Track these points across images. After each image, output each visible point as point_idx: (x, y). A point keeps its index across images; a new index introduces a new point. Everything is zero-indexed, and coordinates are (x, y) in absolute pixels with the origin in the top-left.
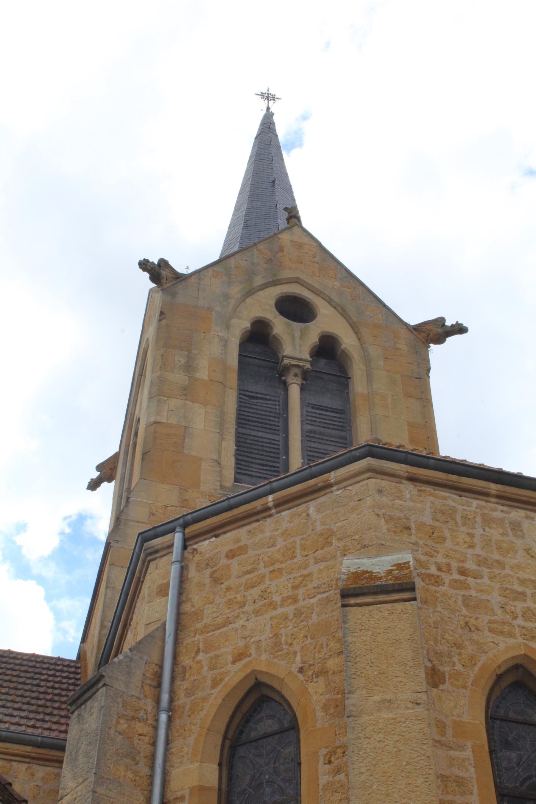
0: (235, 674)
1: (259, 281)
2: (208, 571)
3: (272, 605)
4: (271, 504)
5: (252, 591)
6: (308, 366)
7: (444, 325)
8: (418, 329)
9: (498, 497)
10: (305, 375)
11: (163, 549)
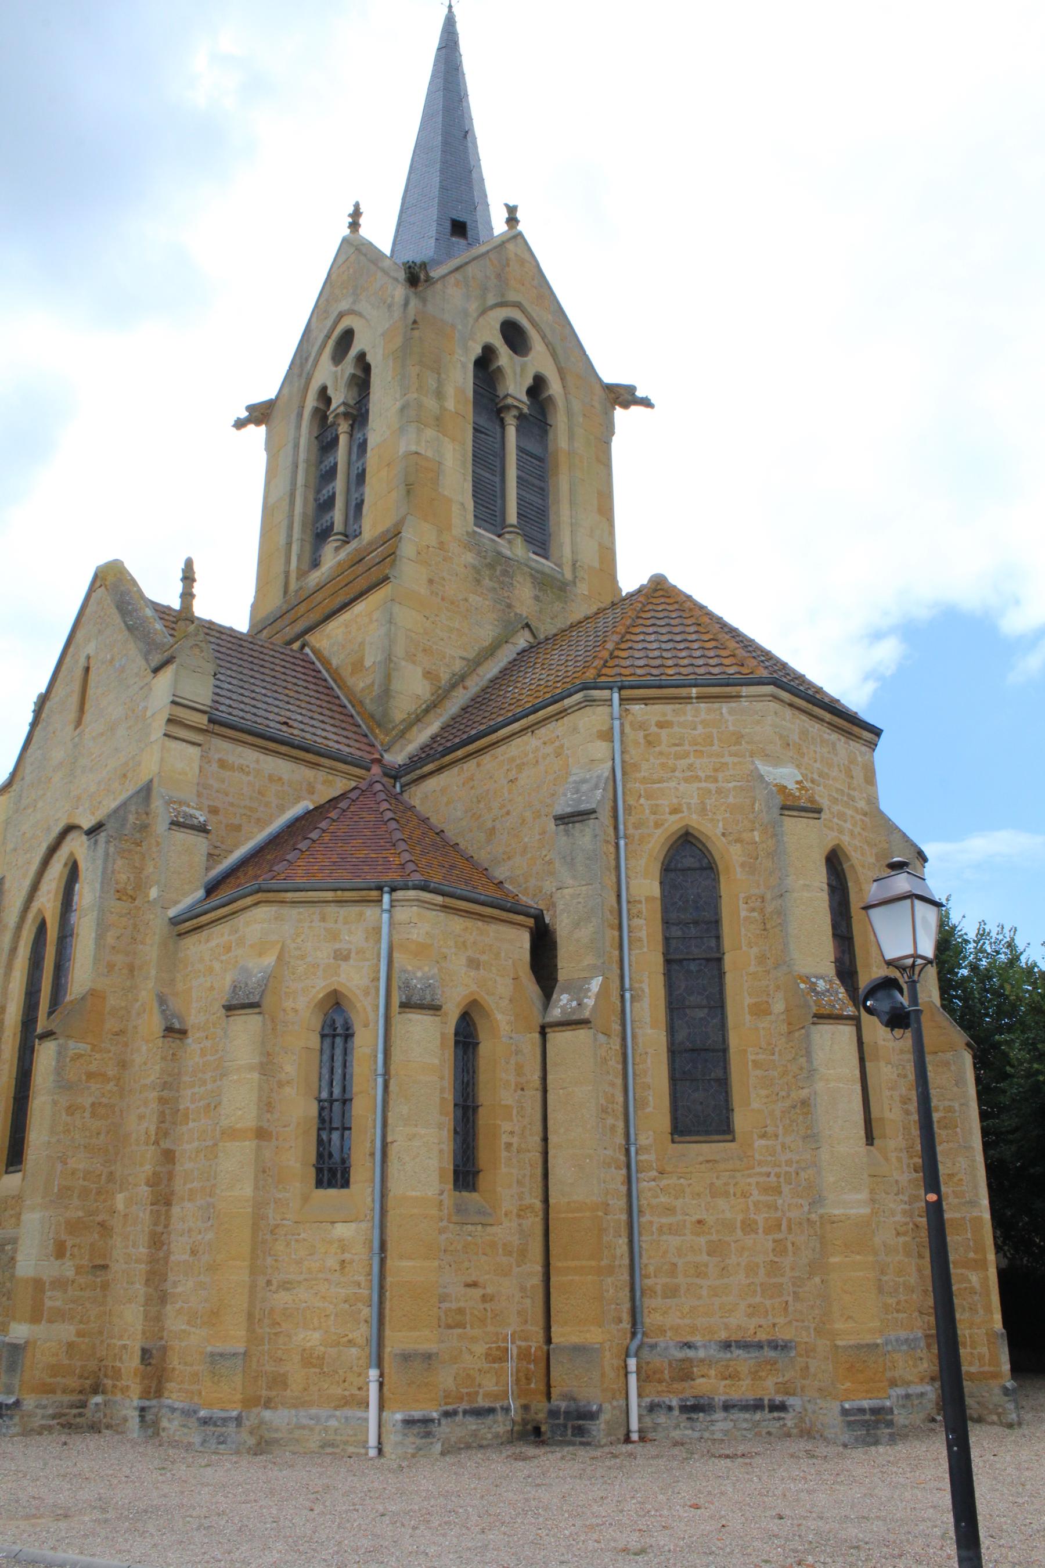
0: (673, 824)
1: (491, 302)
2: (642, 733)
3: (698, 779)
4: (694, 695)
5: (682, 761)
6: (526, 410)
7: (634, 394)
9: (828, 723)
10: (521, 417)
11: (600, 700)
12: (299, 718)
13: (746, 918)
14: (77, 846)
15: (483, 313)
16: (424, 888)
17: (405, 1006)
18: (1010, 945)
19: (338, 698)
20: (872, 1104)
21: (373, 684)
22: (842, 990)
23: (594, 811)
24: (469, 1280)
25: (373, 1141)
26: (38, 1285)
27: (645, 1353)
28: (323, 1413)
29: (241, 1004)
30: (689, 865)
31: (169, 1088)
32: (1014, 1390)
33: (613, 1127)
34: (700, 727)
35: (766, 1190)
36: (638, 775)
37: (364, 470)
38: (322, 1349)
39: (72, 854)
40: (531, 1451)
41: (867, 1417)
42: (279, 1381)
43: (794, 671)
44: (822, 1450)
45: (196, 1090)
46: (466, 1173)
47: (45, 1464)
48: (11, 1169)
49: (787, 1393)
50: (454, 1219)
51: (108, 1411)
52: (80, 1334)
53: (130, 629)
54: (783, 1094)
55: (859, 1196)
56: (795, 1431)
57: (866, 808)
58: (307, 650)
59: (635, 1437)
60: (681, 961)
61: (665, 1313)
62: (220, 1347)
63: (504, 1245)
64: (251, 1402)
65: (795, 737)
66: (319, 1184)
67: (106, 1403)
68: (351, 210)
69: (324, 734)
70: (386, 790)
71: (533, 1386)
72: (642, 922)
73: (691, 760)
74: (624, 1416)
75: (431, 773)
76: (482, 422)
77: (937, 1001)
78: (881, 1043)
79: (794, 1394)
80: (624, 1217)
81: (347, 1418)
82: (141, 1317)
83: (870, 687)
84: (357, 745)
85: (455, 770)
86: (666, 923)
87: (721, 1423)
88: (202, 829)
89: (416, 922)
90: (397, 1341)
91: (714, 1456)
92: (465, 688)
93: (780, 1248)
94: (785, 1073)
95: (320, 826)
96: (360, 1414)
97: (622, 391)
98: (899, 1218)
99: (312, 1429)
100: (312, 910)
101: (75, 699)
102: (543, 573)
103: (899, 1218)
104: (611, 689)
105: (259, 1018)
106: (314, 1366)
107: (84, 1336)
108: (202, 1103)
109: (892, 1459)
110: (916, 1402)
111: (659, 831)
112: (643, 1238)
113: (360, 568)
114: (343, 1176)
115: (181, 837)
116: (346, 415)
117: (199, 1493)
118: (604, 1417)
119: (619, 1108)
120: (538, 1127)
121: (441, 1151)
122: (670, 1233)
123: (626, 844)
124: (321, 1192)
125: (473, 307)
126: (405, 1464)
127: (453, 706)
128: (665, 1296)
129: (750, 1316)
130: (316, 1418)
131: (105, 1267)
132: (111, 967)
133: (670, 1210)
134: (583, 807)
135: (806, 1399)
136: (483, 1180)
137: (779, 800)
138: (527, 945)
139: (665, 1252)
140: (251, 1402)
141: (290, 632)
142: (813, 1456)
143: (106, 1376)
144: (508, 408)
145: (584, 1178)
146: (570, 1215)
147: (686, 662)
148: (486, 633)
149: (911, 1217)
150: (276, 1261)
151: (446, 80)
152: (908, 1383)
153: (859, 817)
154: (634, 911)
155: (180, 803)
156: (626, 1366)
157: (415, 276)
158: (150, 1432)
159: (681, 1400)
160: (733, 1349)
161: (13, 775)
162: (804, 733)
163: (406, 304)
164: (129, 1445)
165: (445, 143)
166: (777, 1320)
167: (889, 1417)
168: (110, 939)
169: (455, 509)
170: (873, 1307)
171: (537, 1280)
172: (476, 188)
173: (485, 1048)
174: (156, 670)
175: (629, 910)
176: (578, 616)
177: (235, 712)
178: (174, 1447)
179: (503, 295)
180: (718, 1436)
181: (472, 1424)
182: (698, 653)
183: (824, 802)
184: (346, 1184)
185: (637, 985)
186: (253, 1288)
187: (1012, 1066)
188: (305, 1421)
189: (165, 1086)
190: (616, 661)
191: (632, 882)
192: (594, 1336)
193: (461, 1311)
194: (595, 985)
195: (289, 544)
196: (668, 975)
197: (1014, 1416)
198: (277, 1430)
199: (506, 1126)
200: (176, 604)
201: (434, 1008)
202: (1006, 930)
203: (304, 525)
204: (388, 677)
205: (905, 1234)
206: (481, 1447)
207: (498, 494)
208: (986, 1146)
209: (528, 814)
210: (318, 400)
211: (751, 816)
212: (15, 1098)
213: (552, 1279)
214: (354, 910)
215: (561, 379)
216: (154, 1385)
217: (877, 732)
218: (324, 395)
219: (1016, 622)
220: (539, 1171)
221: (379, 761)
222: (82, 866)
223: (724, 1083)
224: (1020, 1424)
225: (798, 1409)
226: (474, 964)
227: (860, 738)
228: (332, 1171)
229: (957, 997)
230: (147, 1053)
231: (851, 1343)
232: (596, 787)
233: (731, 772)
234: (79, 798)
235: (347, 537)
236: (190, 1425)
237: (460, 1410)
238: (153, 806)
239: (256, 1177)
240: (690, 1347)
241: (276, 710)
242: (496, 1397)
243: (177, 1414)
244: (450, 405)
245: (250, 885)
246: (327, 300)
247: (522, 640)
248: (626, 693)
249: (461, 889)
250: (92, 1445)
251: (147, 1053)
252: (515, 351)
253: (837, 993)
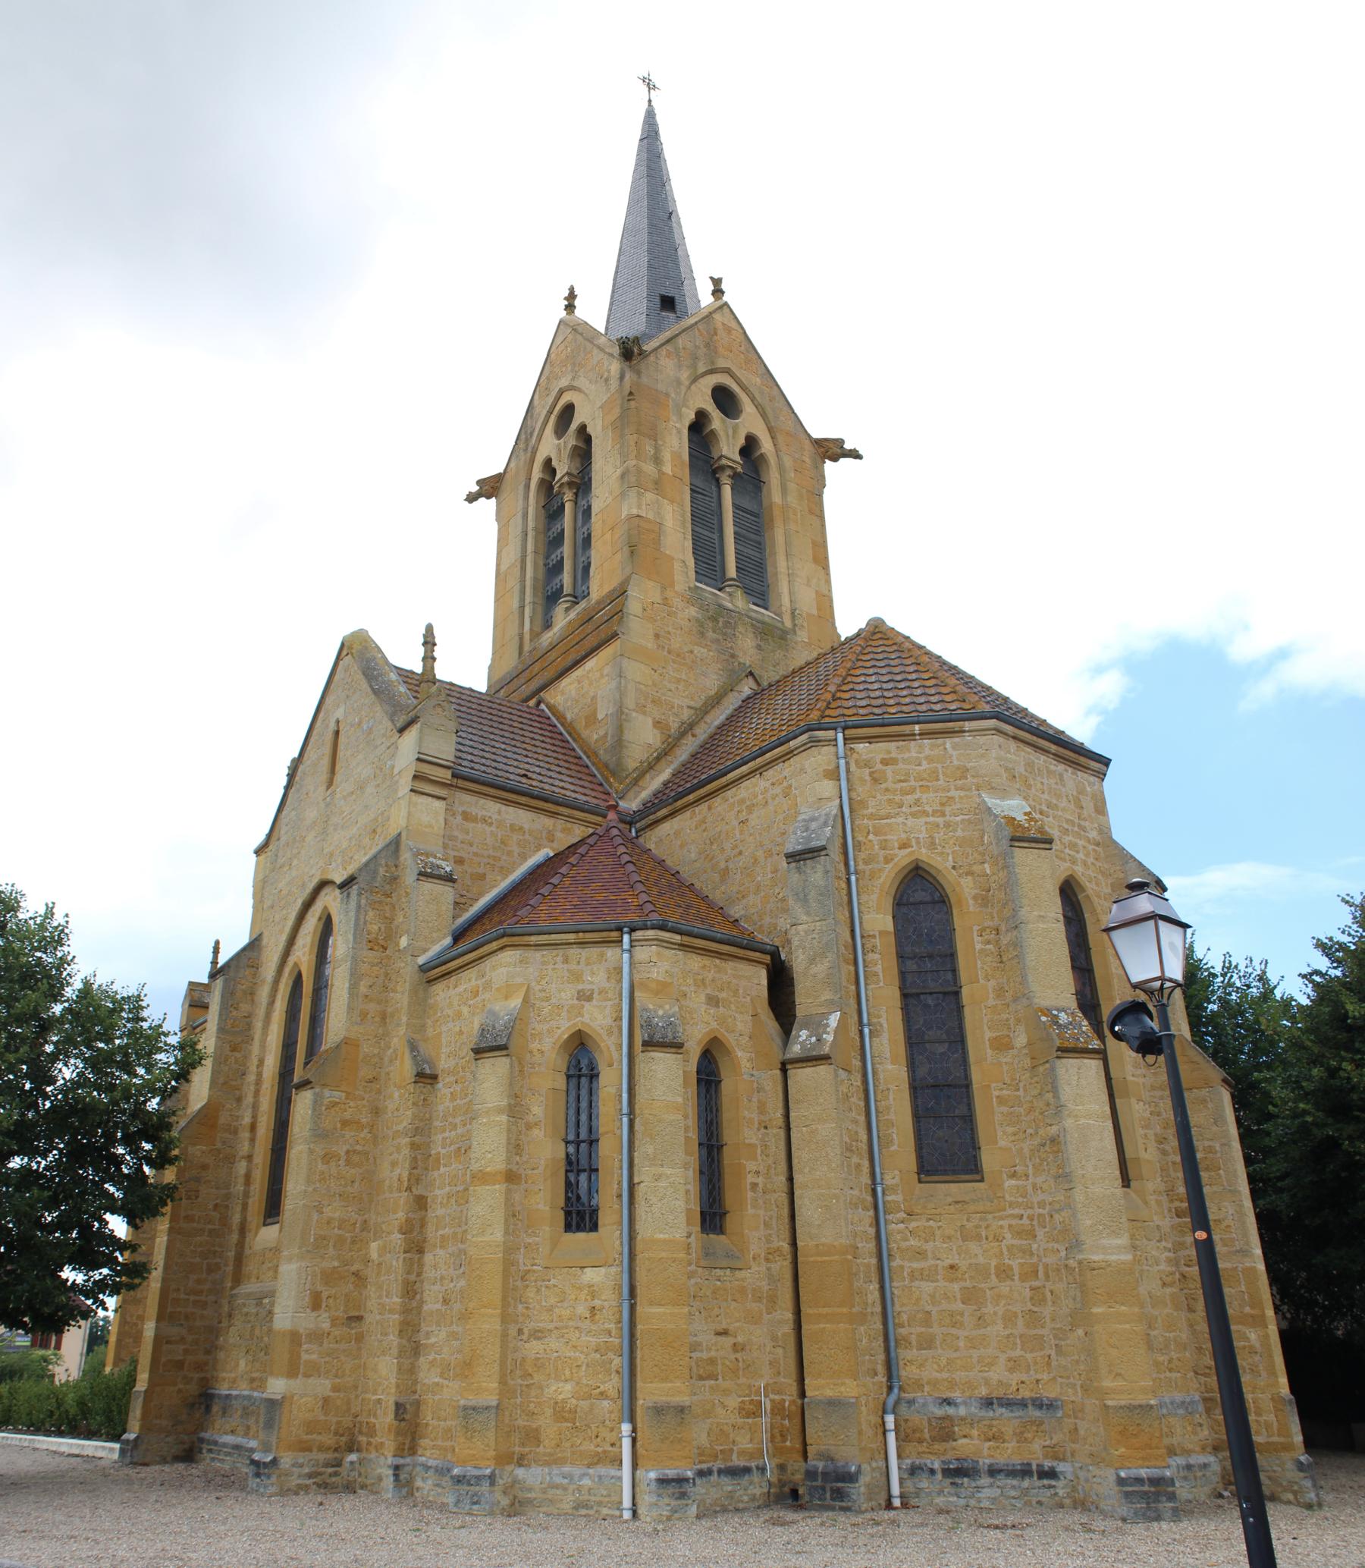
0: (903, 858)
1: (702, 369)
2: (867, 771)
3: (925, 813)
6: (739, 470)
8: (819, 443)
10: (736, 476)
12: (538, 770)
13: (982, 951)
14: (330, 900)
15: (695, 380)
16: (662, 927)
17: (648, 1044)
18: (1262, 978)
19: (574, 750)
20: (1125, 1144)
21: (606, 735)
22: (1085, 1023)
23: (823, 848)
24: (720, 1328)
25: (620, 1183)
26: (295, 1338)
27: (903, 1409)
28: (577, 1471)
29: (488, 1047)
30: (920, 897)
31: (421, 1130)
32: (1310, 1465)
33: (858, 1166)
34: (924, 762)
35: (1018, 1233)
36: (865, 812)
37: (589, 535)
38: (574, 1401)
39: (326, 908)
40: (790, 1516)
41: (1146, 1488)
42: (533, 1436)
43: (1016, 705)
44: (1099, 1524)
45: (447, 1134)
46: (712, 1215)
47: (303, 1524)
48: (269, 1221)
49: (1057, 1459)
50: (703, 1263)
51: (363, 1471)
52: (336, 1389)
53: (375, 692)
54: (1030, 1131)
55: (1119, 1242)
56: (1067, 1501)
57: (1098, 838)
58: (543, 706)
59: (897, 1502)
60: (918, 995)
61: (921, 1365)
62: (473, 1400)
63: (754, 1290)
64: (505, 1459)
65: (1021, 769)
66: (568, 1228)
67: (360, 1461)
68: (566, 293)
69: (562, 784)
70: (622, 834)
71: (788, 1443)
72: (877, 956)
73: (918, 795)
74: (884, 1479)
75: (665, 818)
76: (699, 483)
77: (1188, 1035)
78: (1130, 1078)
79: (1064, 1460)
80: (874, 1261)
81: (600, 1477)
82: (395, 1369)
83: (1094, 721)
84: (593, 794)
85: (688, 814)
86: (901, 957)
87: (988, 1490)
88: (449, 879)
89: (655, 960)
90: (650, 1392)
91: (981, 1526)
92: (694, 736)
93: (1038, 1296)
94: (1031, 1109)
95: (531, 902)
96: (613, 1472)
98: (1163, 1267)
99: (565, 1489)
100: (555, 952)
101: (326, 762)
102: (763, 623)
103: (1163, 1267)
104: (835, 729)
105: (506, 1060)
106: (566, 1421)
107: (339, 1391)
108: (452, 1148)
109: (1177, 1537)
110: (1199, 1474)
111: (890, 865)
112: (895, 1284)
113: (590, 627)
114: (591, 1218)
115: (429, 887)
116: (570, 484)
117: (454, 1556)
118: (864, 1479)
119: (864, 1147)
120: (783, 1166)
121: (687, 1192)
122: (922, 1279)
123: (857, 880)
124: (570, 1235)
125: (685, 376)
126: (660, 1527)
127: (683, 754)
128: (920, 1348)
129: (1011, 1370)
130: (569, 1476)
131: (360, 1318)
132: (364, 1015)
133: (921, 1254)
134: (814, 844)
135: (1077, 1465)
136: (730, 1222)
137: (1008, 832)
138: (765, 982)
139: (918, 1299)
140: (505, 1459)
141: (526, 690)
142: (1090, 1530)
143: (360, 1432)
144: (722, 468)
145: (831, 1219)
146: (819, 1259)
147: (907, 700)
148: (712, 683)
149: (1177, 1265)
150: (527, 1308)
151: (649, 168)
152: (1188, 1452)
153: (1091, 847)
154: (868, 946)
155: (427, 855)
156: (884, 1423)
157: (629, 350)
158: (404, 1491)
159: (943, 1462)
160: (995, 1406)
161: (269, 836)
162: (1029, 765)
163: (622, 378)
164: (383, 1506)
165: (651, 225)
166: (1039, 1377)
167: (1170, 1489)
168: (363, 989)
169: (677, 566)
170: (1139, 1360)
171: (788, 1328)
172: (682, 264)
173: (728, 1086)
174: (401, 731)
175: (863, 945)
176: (800, 662)
177: (477, 767)
178: (428, 1508)
179: (713, 363)
180: (986, 1504)
181: (728, 1484)
182: (919, 692)
183: (1055, 833)
184: (594, 1227)
185: (875, 1020)
186: (504, 1335)
187: (1275, 1106)
188: (558, 1480)
189: (417, 1131)
190: (839, 703)
191: (865, 917)
192: (849, 1389)
193: (712, 1361)
194: (834, 1020)
195: (522, 607)
196: (906, 1010)
197: (1312, 1495)
198: (530, 1490)
199: (751, 1166)
200: (418, 668)
201: (676, 1046)
202: (1256, 963)
203: (535, 588)
204: (620, 729)
205: (1172, 1284)
206: (737, 1510)
208: (1255, 1194)
209: (760, 854)
210: (543, 472)
211: (981, 849)
212: (272, 1150)
213: (804, 1327)
214: (594, 952)
216: (407, 1442)
217: (1106, 762)
218: (549, 467)
219: (1244, 649)
220: (786, 1212)
221: (615, 807)
222: (335, 919)
223: (969, 1119)
224: (1320, 1505)
225: (1069, 1477)
226: (713, 1001)
228: (580, 1216)
229: (1207, 1033)
230: (399, 1101)
231: (1123, 1403)
232: (825, 824)
233: (958, 806)
234: (332, 855)
235: (576, 598)
236: (444, 1484)
237: (715, 1469)
238: (402, 859)
239: (506, 1220)
240: (949, 1404)
241: (516, 763)
242: (752, 1456)
243: (431, 1473)
244: (668, 469)
245: (495, 931)
246: (548, 378)
247: (747, 688)
248: (849, 732)
249: (698, 927)
250: (347, 1505)
251: (399, 1101)
252: (727, 415)
253: (1081, 1026)
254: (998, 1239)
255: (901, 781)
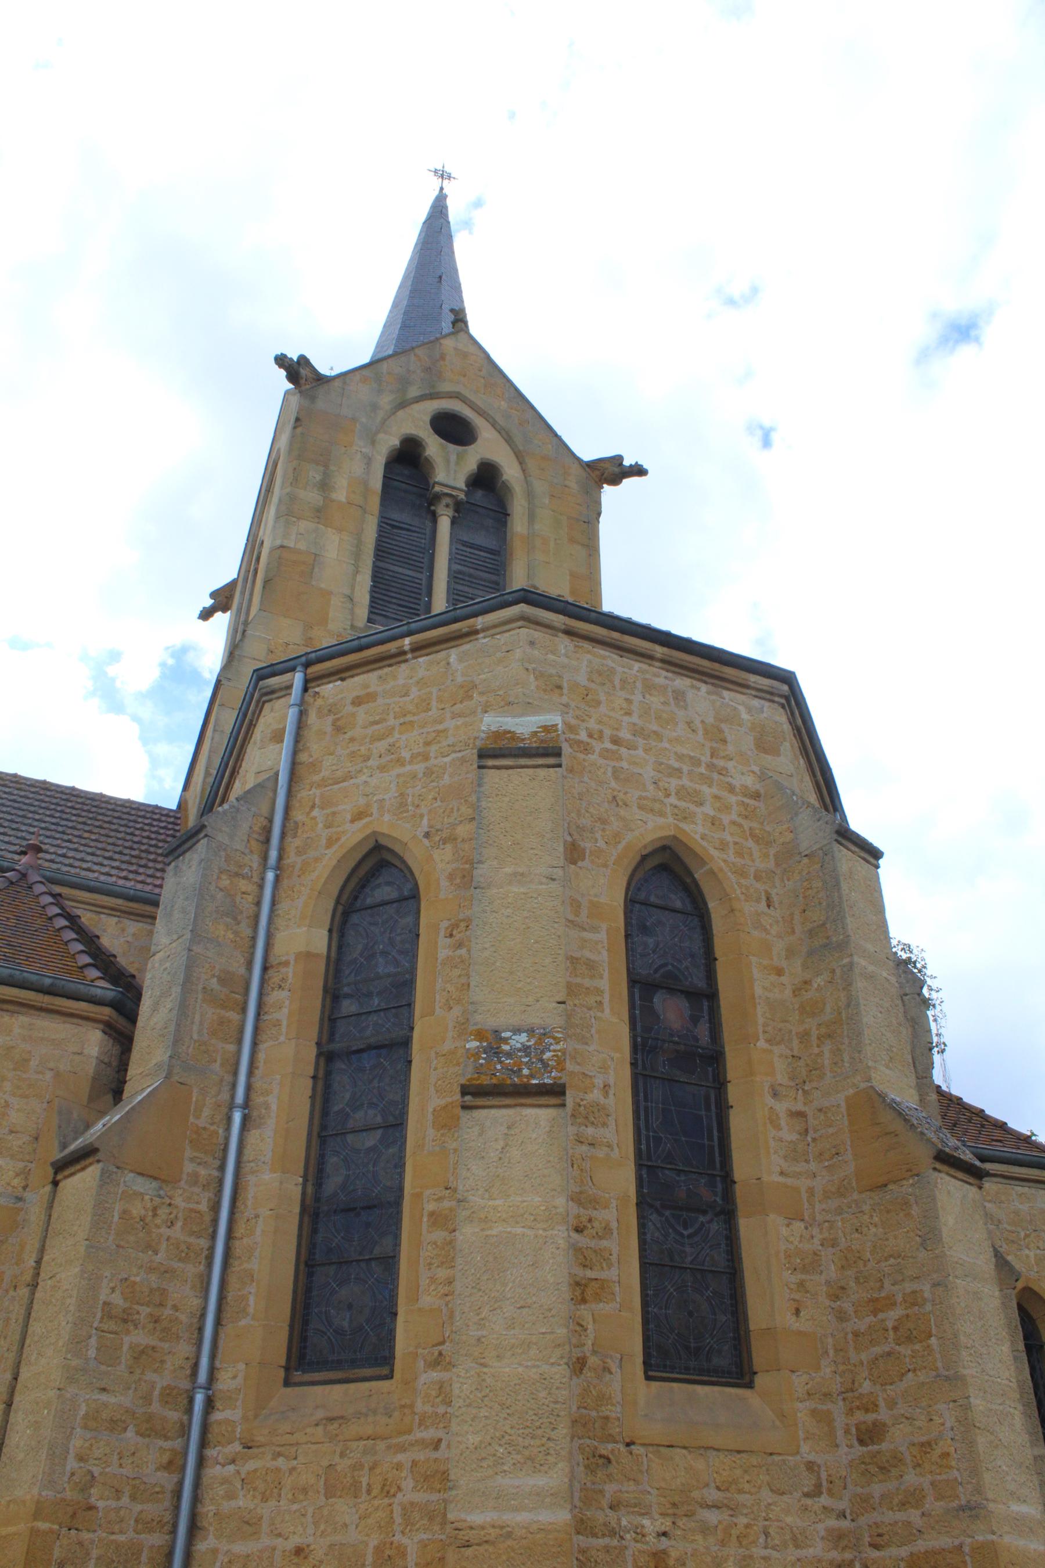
1: (413, 392)
3: (400, 761)
9: (662, 661)
10: (458, 506)
11: (281, 689)
55: (540, 1481)
72: (283, 994)
97: (607, 465)
207: (424, 591)
215: (521, 463)
227: (748, 687)
244: (340, 495)
254: (388, 1490)
255: (377, 723)
